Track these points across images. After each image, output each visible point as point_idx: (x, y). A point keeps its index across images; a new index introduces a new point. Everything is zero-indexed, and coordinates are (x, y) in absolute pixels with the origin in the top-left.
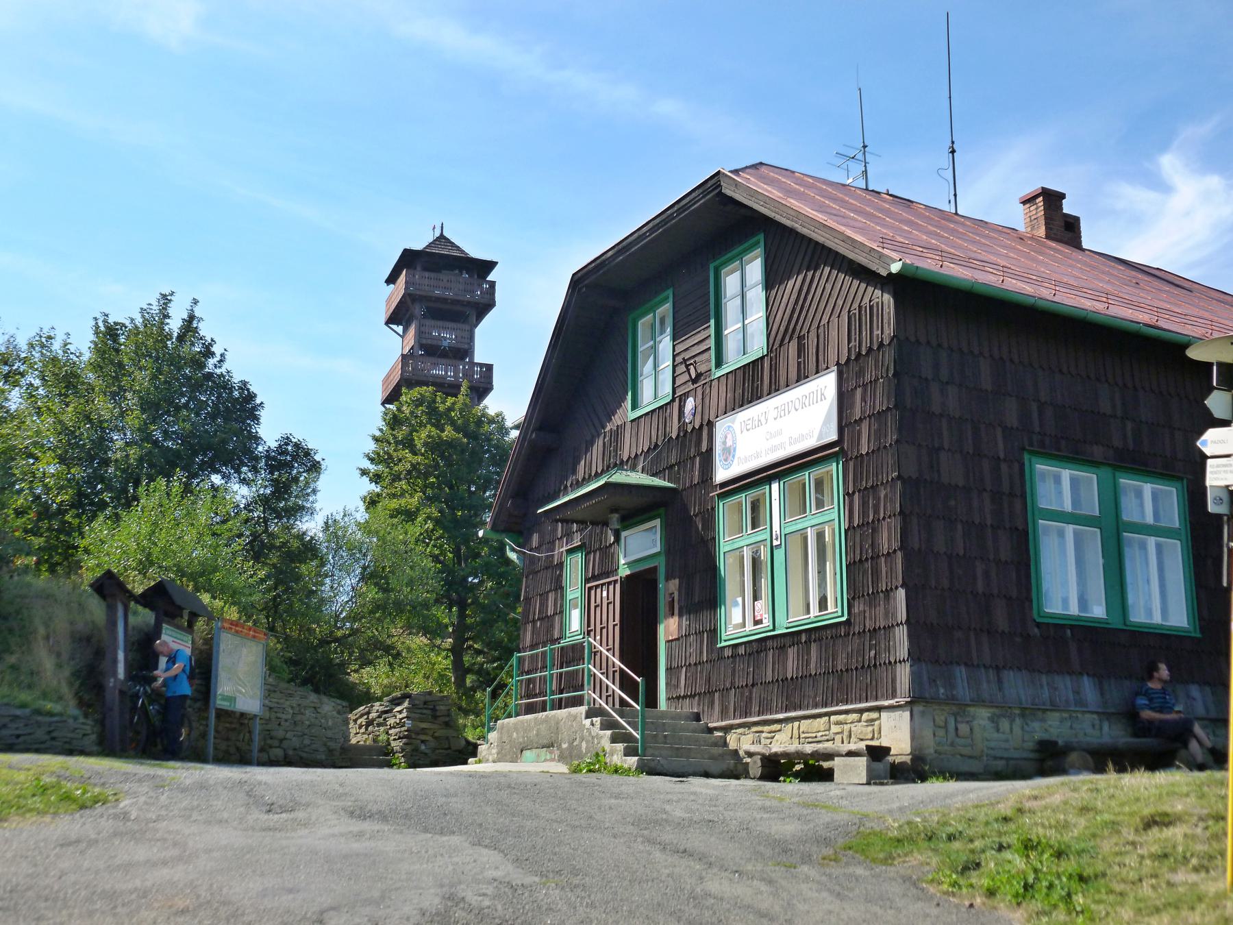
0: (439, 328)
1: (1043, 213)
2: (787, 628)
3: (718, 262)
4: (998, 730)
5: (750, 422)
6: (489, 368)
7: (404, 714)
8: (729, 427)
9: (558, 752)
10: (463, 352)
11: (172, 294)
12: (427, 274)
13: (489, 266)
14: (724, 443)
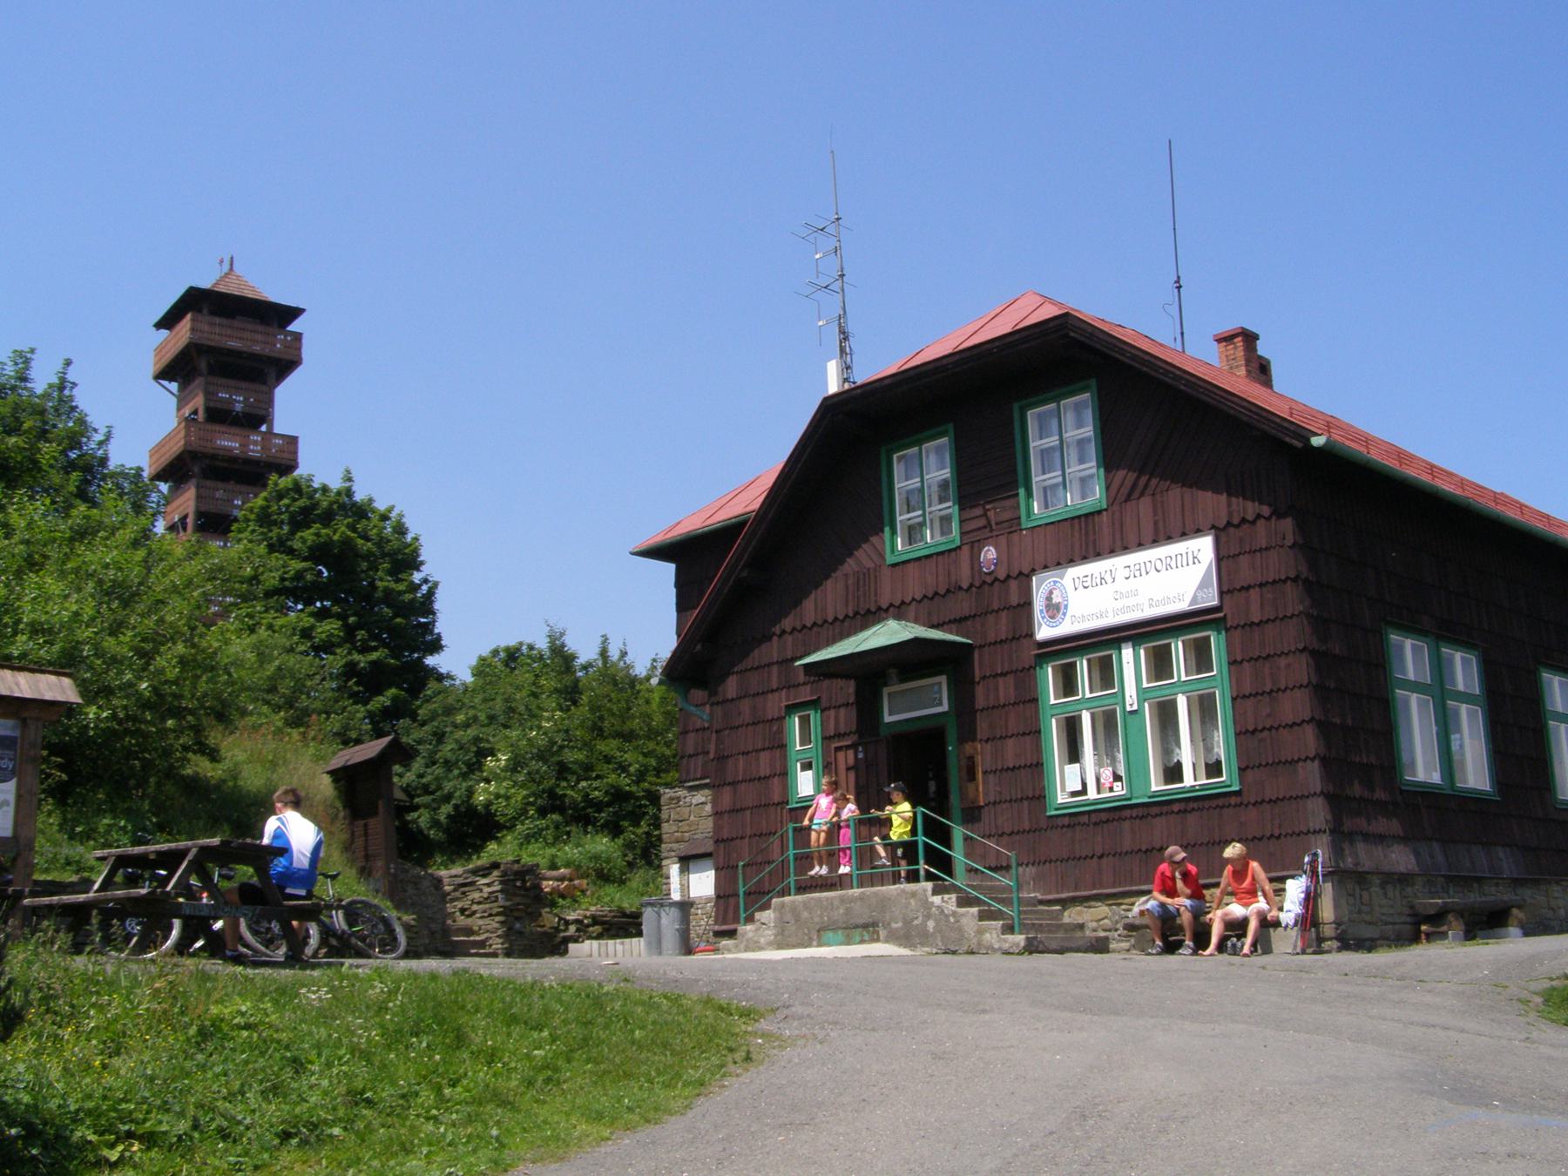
0: (227, 388)
1: (1242, 354)
2: (1150, 797)
3: (1024, 402)
4: (1386, 897)
5: (1089, 579)
6: (292, 441)
7: (497, 887)
8: (1055, 582)
9: (885, 932)
10: (257, 418)
11: (32, 351)
12: (217, 320)
13: (294, 313)
14: (1049, 598)
